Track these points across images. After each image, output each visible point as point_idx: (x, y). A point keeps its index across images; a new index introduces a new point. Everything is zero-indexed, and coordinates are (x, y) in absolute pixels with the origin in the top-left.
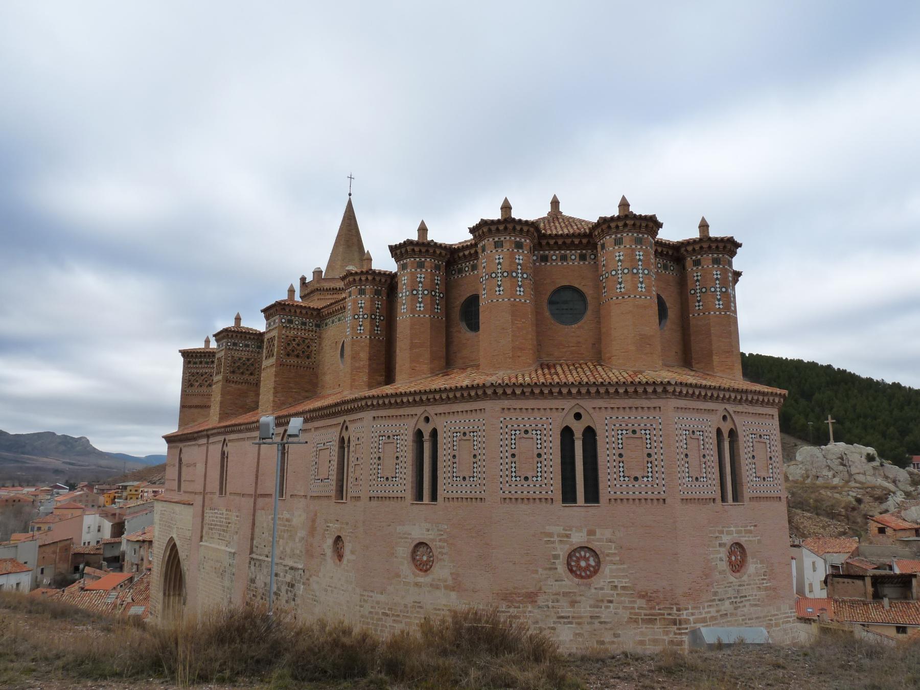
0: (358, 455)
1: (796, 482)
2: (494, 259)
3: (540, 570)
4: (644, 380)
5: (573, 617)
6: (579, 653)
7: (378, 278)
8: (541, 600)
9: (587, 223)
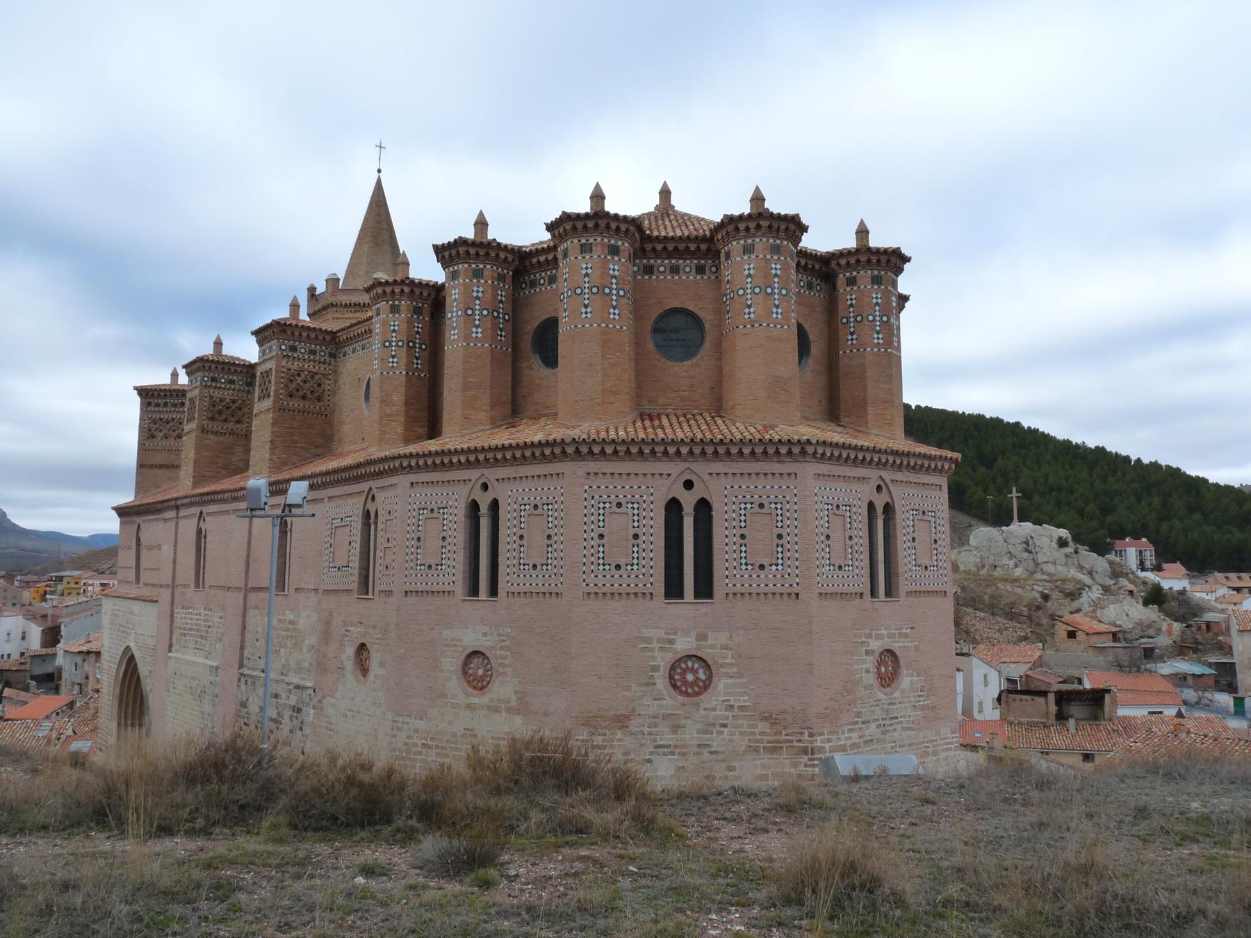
0: (389, 535)
1: (967, 572)
2: (580, 267)
3: (634, 687)
4: (777, 438)
5: (675, 746)
6: (675, 790)
7: (417, 291)
8: (634, 725)
9: (708, 222)
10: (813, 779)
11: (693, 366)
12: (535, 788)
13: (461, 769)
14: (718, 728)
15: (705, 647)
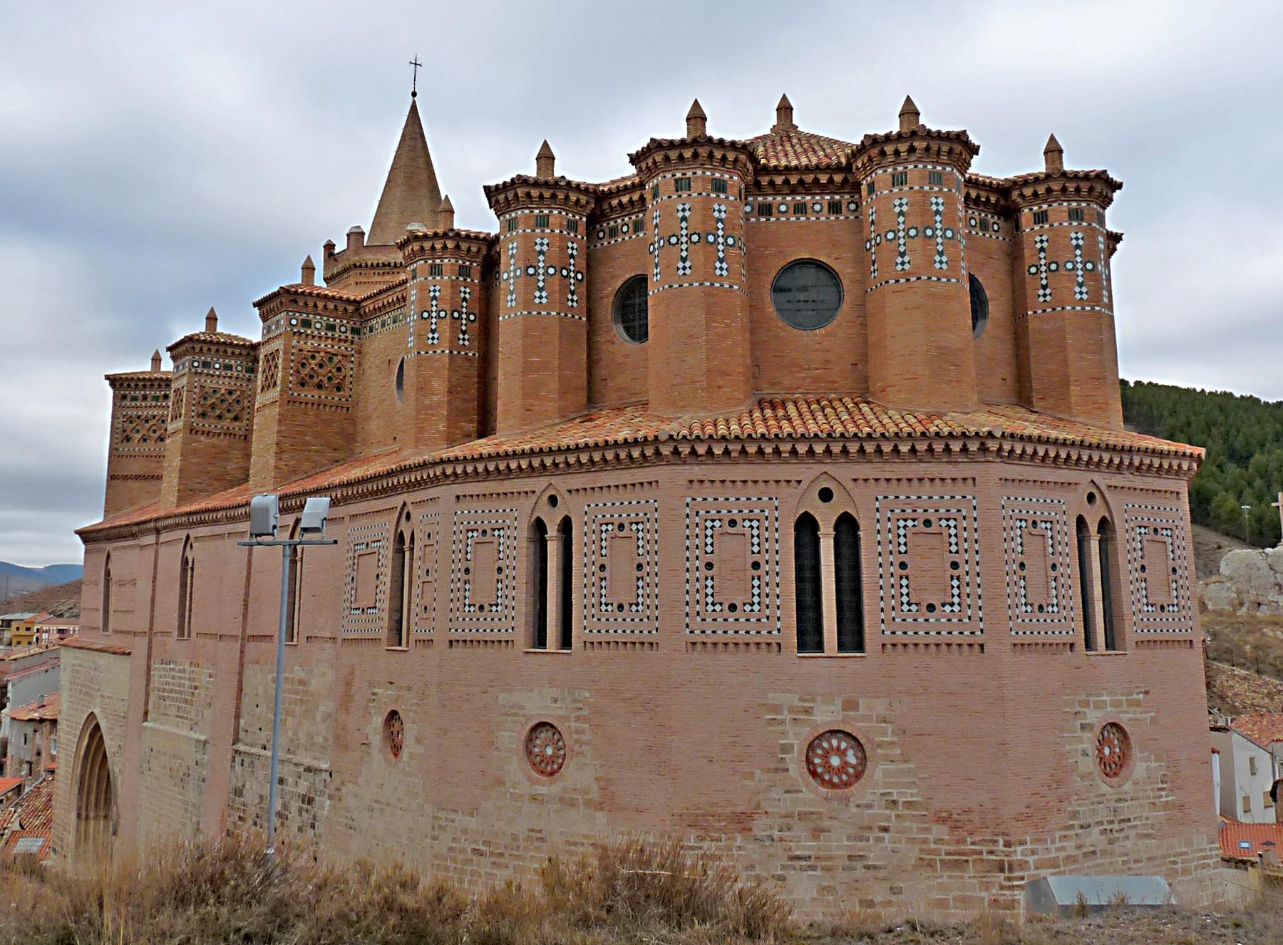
1: (1220, 613)
2: (670, 207)
6: (829, 923)
11: (828, 335)
15: (854, 719)
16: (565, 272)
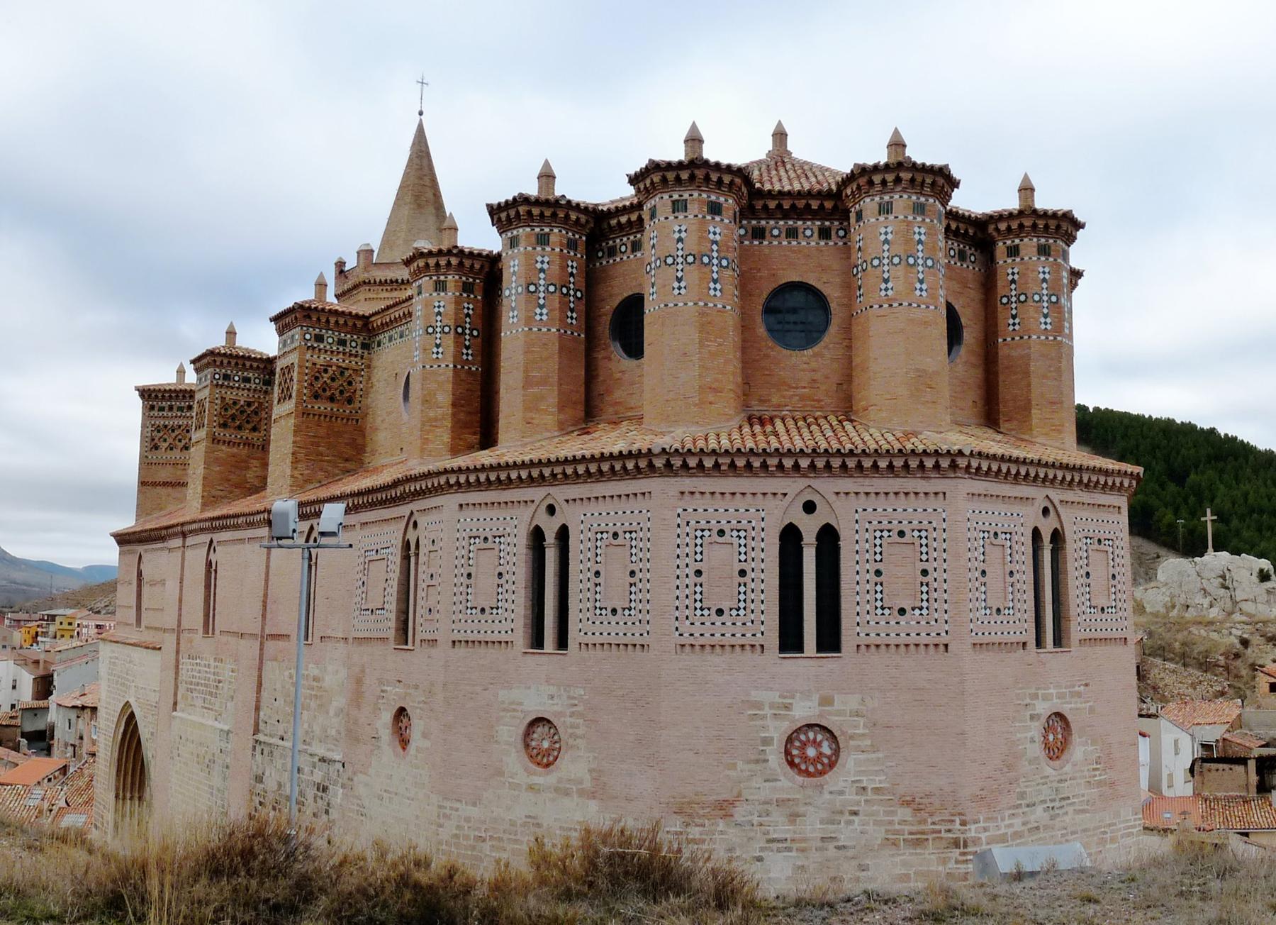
0: (432, 570)
1: (1156, 615)
2: (673, 230)
3: (740, 765)
4: (921, 448)
5: (793, 840)
6: (792, 897)
7: (467, 263)
8: (740, 813)
9: (834, 173)
10: (966, 879)
11: (815, 355)
12: (614, 893)
13: (522, 868)
14: (847, 817)
15: (830, 714)
16: (565, 290)
